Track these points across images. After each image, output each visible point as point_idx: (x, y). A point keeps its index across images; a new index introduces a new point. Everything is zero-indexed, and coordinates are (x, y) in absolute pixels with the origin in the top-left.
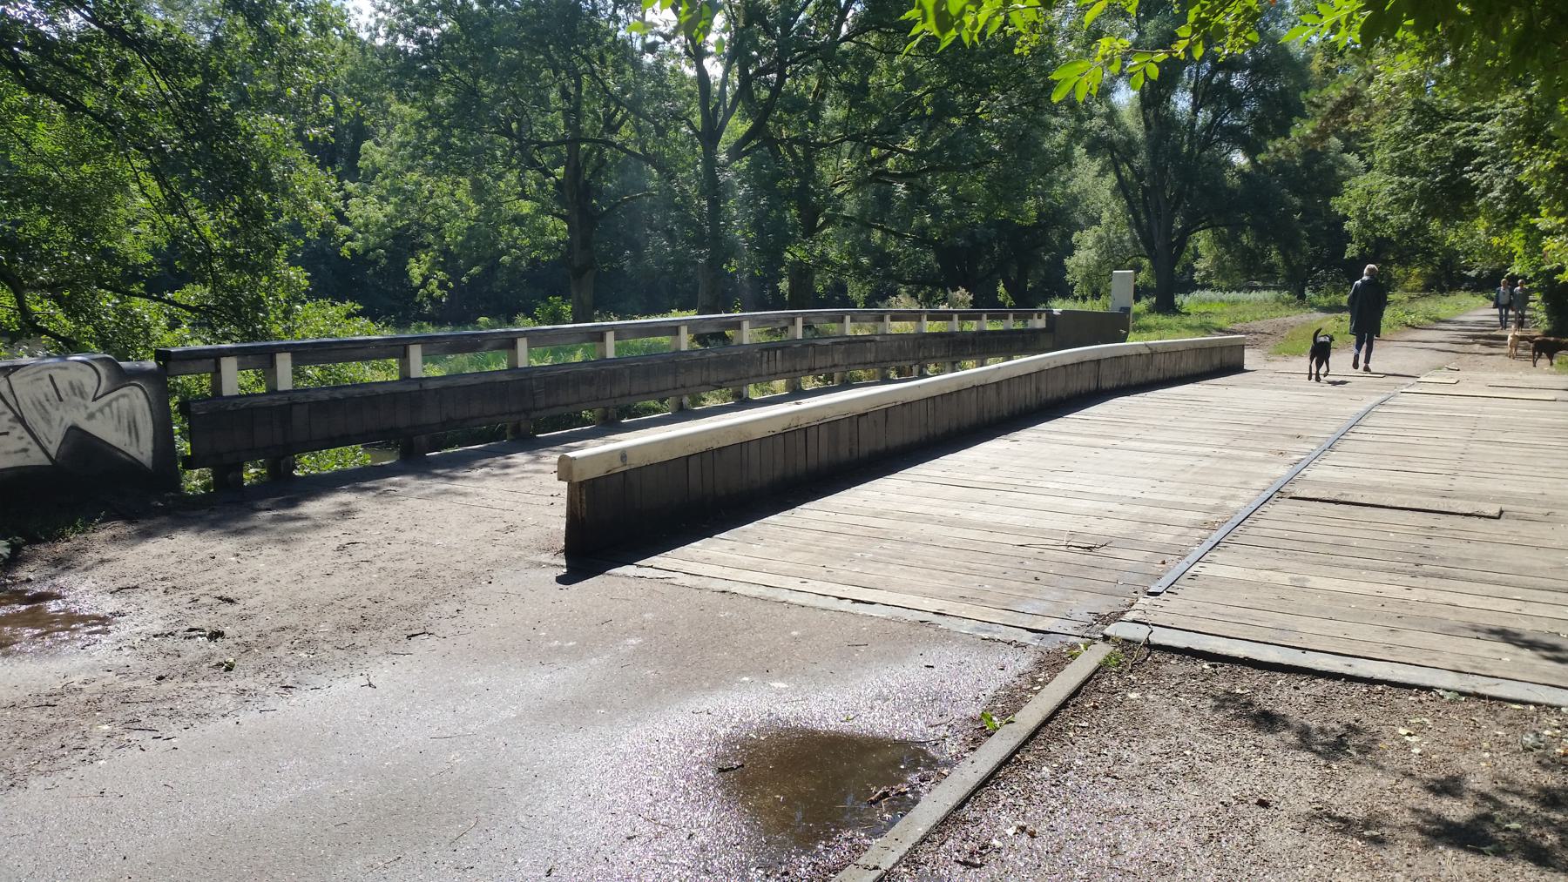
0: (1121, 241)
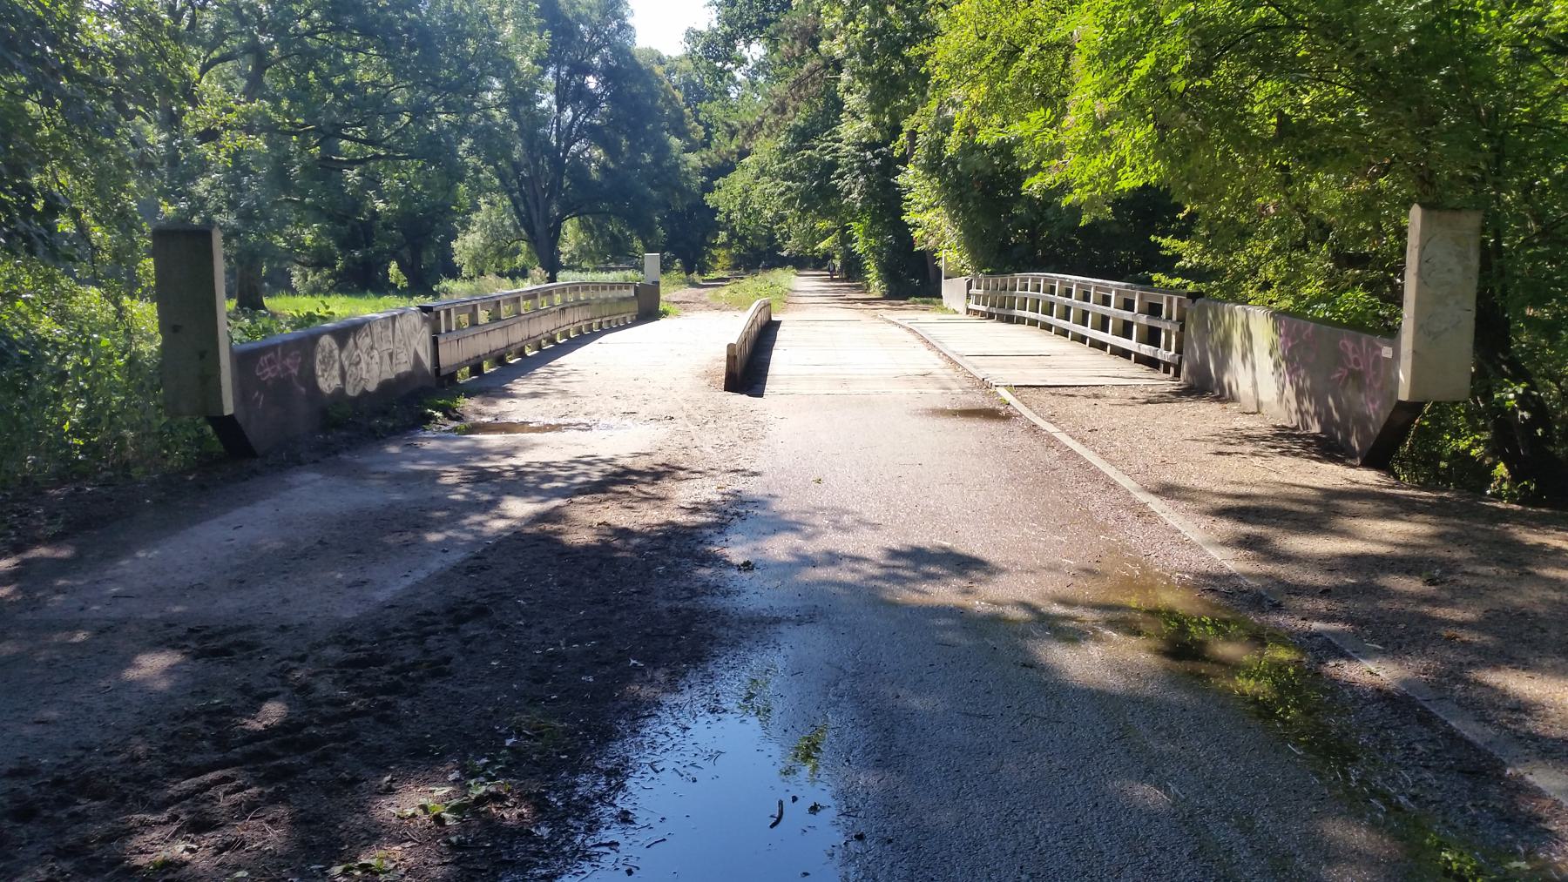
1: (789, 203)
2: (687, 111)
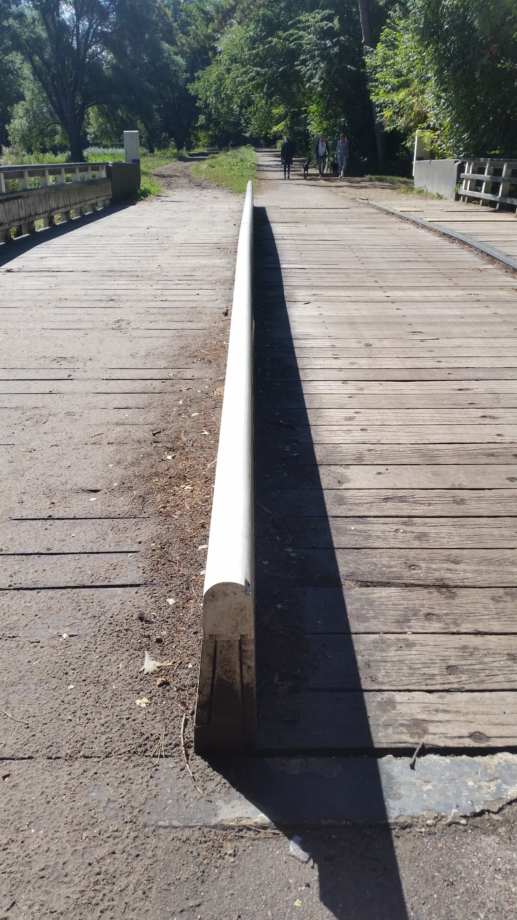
0: (42, 113)
1: (258, 87)
2: (175, 24)
